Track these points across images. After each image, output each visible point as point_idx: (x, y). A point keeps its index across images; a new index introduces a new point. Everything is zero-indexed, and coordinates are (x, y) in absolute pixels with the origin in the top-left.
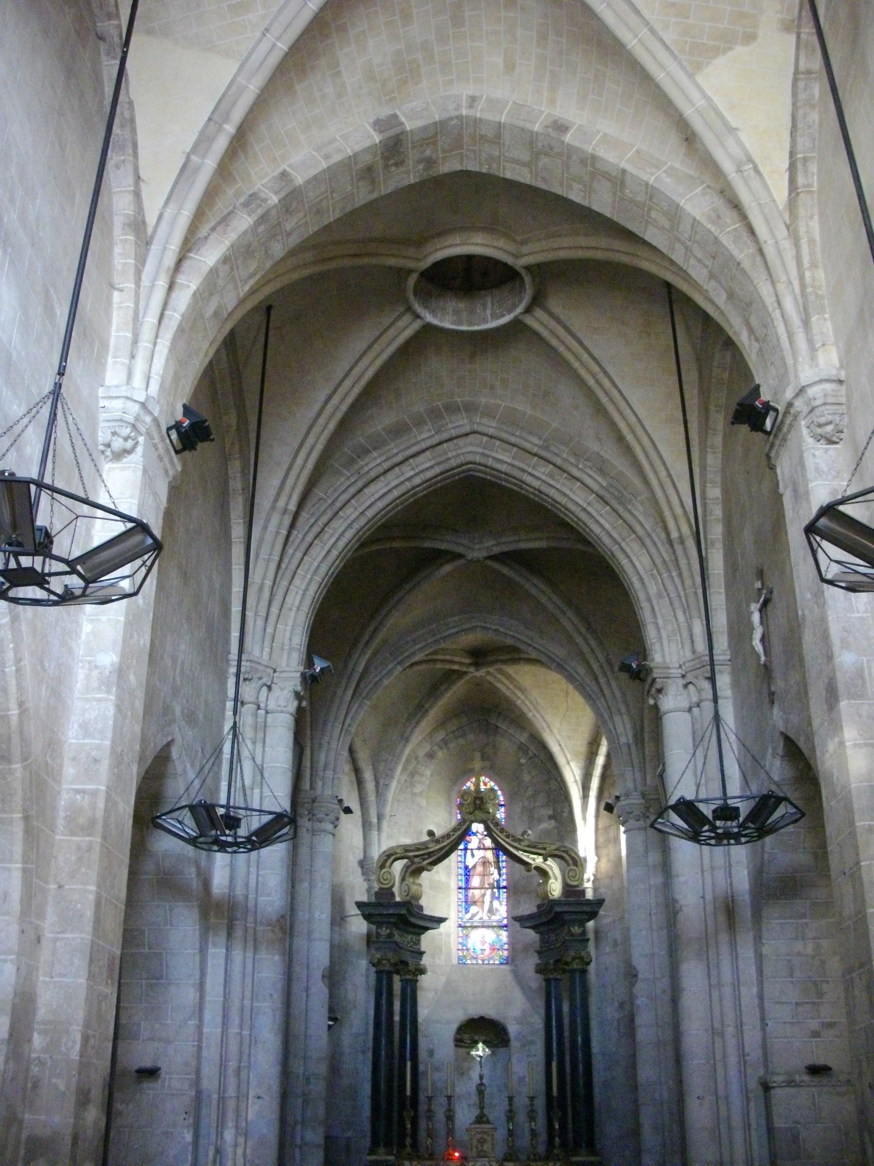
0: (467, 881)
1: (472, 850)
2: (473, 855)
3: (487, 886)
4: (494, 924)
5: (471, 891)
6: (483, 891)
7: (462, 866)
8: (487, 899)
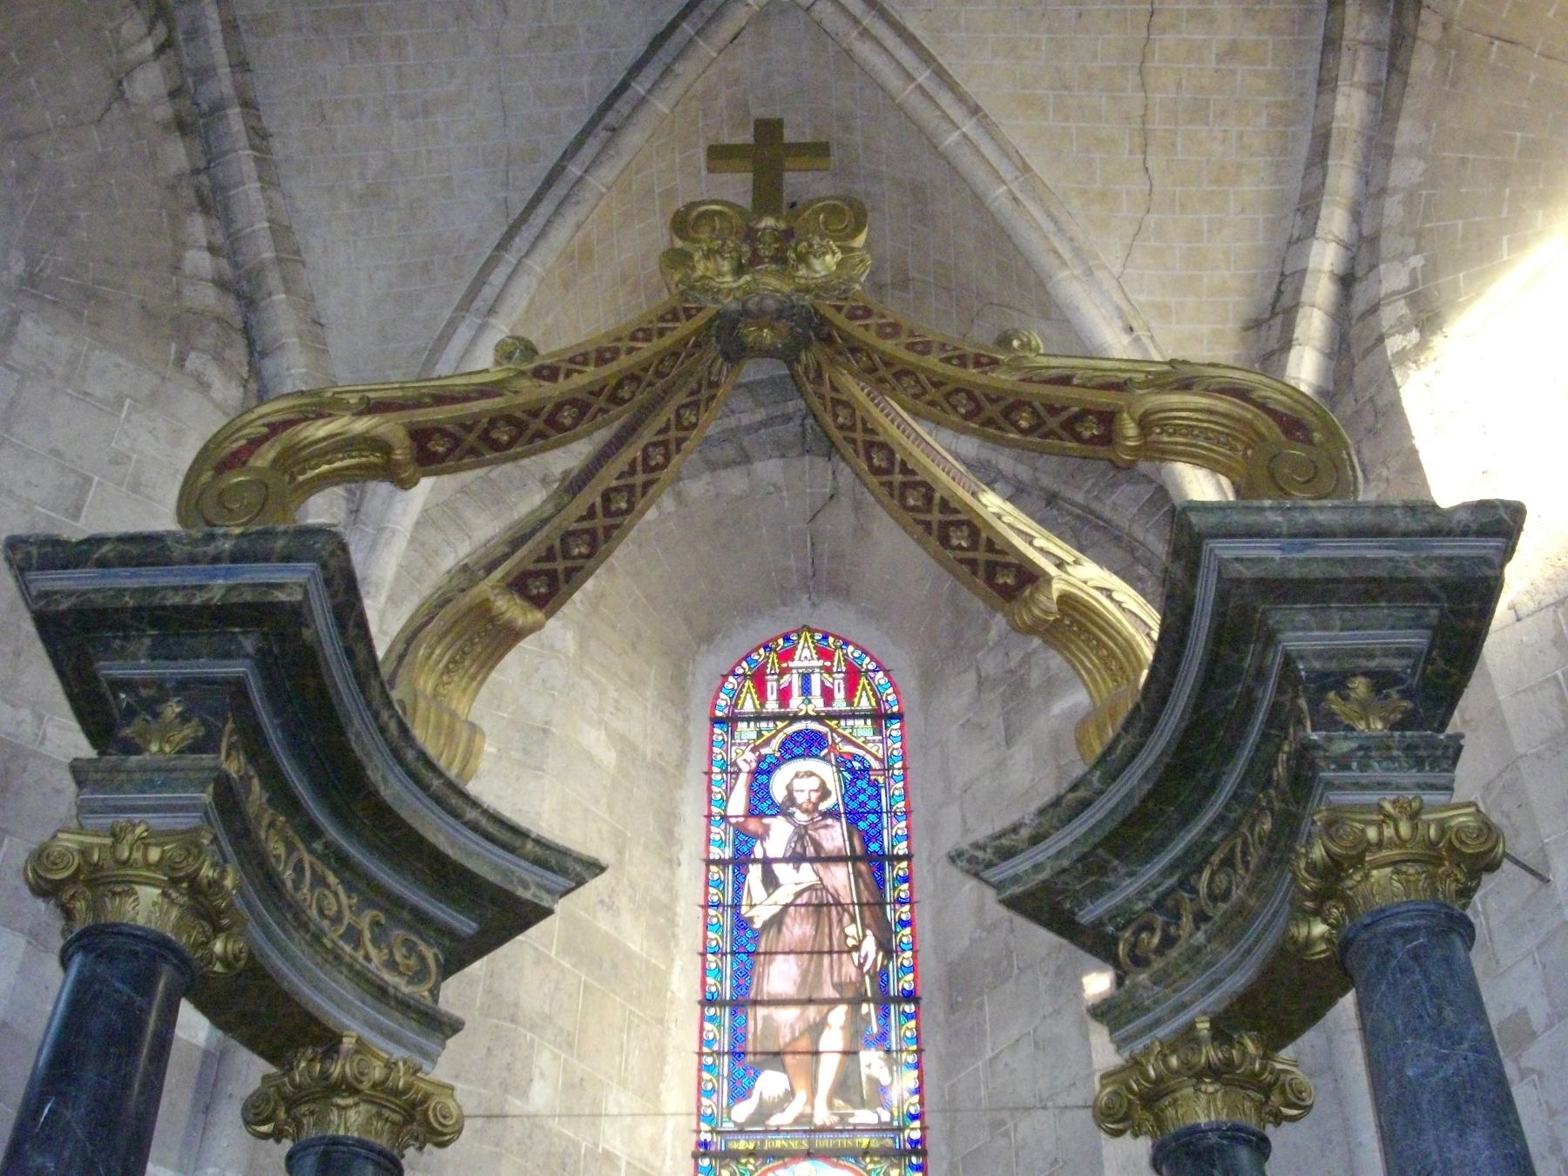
0: (743, 976)
1: (767, 863)
2: (771, 882)
3: (829, 992)
4: (864, 1141)
5: (762, 1012)
6: (812, 1012)
7: (728, 920)
8: (833, 1039)
